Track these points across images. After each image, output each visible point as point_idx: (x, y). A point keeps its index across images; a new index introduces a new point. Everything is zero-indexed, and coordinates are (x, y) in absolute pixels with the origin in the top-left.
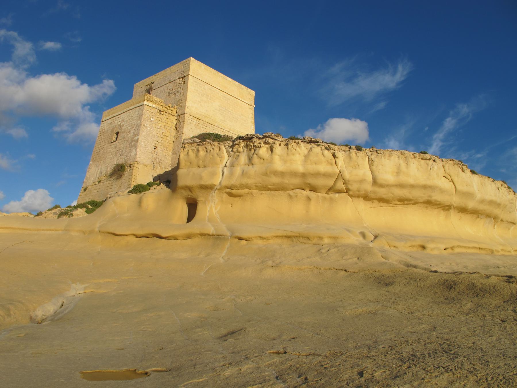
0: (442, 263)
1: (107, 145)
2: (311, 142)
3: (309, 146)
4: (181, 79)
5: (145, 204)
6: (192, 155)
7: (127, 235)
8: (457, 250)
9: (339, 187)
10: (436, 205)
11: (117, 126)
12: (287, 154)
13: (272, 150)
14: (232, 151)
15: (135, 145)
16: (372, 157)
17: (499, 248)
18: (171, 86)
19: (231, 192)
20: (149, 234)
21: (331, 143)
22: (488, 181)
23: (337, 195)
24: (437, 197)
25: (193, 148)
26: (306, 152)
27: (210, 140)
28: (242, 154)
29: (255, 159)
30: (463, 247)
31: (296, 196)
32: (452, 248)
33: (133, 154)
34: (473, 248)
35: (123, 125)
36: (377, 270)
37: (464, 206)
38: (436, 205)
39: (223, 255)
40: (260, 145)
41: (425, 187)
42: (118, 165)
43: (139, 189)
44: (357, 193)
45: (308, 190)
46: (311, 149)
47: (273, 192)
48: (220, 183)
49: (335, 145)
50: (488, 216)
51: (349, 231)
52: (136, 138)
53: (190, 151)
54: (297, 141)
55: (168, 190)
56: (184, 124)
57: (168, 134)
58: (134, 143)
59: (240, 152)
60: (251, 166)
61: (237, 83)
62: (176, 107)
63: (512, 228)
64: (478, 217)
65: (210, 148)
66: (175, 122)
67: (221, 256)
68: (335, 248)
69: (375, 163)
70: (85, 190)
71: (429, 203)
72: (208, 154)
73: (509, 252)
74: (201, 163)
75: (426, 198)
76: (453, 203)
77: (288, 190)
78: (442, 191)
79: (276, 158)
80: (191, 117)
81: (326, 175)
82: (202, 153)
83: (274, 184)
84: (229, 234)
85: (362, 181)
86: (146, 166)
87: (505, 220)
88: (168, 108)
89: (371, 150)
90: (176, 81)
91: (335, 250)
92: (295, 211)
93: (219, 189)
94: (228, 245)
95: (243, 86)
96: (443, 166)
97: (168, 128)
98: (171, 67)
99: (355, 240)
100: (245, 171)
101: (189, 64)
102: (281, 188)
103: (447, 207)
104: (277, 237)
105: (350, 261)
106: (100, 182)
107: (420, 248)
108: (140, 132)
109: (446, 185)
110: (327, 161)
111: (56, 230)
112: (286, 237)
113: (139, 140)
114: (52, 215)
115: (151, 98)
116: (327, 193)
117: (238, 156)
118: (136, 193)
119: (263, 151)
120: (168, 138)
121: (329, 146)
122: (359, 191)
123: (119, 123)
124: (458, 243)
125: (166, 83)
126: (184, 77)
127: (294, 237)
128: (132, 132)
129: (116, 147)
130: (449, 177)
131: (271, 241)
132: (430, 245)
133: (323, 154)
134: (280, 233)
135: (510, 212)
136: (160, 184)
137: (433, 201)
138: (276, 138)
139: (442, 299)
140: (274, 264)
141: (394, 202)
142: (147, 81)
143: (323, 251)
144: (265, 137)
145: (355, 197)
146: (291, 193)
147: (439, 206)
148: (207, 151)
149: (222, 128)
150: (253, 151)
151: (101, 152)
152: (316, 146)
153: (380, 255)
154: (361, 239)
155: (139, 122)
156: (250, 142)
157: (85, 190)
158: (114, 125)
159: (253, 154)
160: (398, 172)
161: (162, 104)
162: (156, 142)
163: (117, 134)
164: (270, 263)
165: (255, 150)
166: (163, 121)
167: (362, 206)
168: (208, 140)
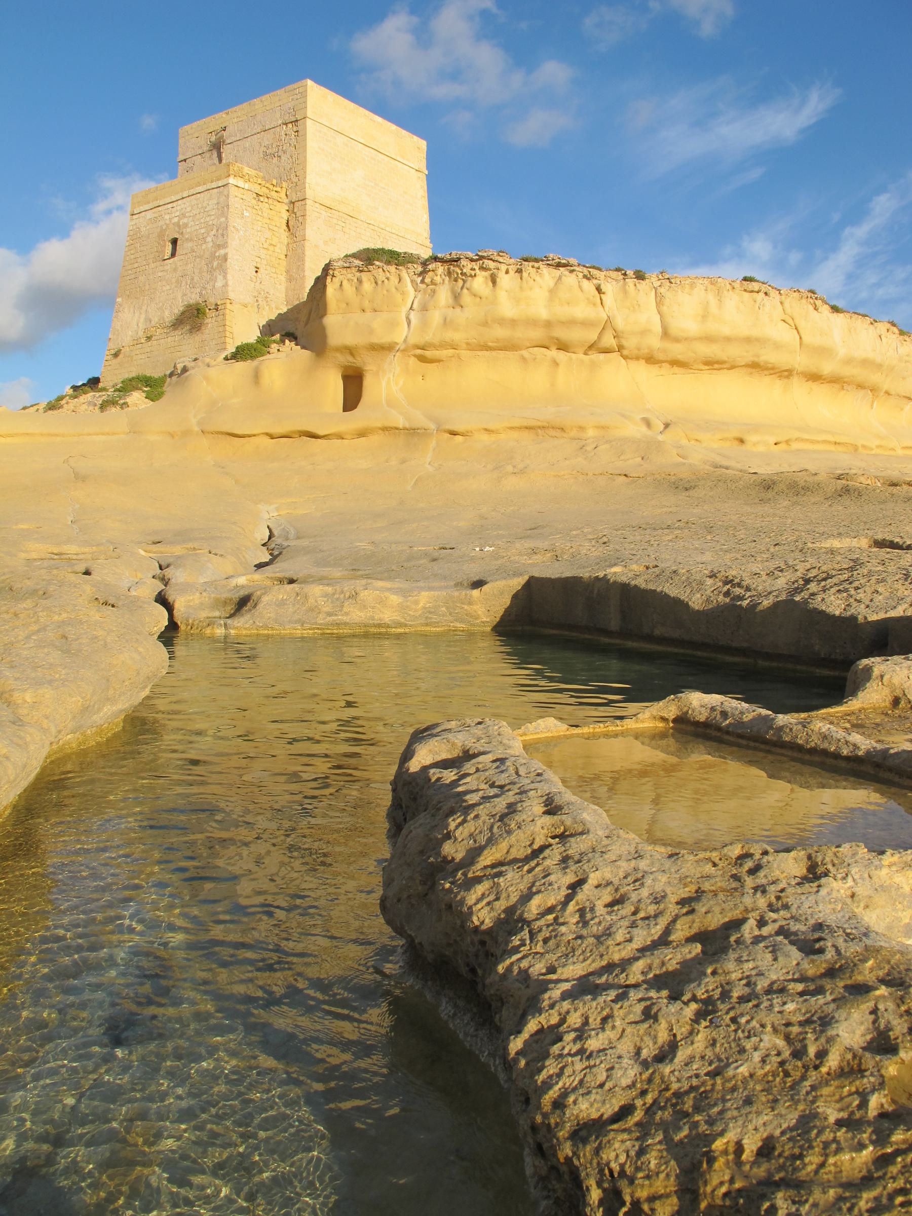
0: (768, 464)
1: (152, 265)
2: (559, 265)
3: (557, 273)
4: (290, 126)
5: (266, 380)
6: (348, 288)
7: (254, 435)
8: (795, 446)
9: (606, 344)
10: (767, 369)
11: (171, 226)
12: (521, 288)
13: (494, 282)
14: (423, 282)
15: (220, 266)
16: (662, 290)
17: (874, 443)
18: (267, 139)
19: (424, 355)
20: (294, 432)
21: (594, 267)
22: (861, 324)
23: (602, 356)
24: (768, 356)
25: (350, 276)
26: (551, 283)
27: (382, 261)
28: (442, 288)
29: (466, 298)
30: (807, 440)
31: (535, 359)
32: (787, 442)
33: (219, 284)
34: (825, 442)
35: (186, 225)
36: (672, 474)
37: (815, 370)
38: (767, 369)
39: (429, 460)
40: (473, 273)
41: (748, 340)
42: (189, 306)
43: (242, 353)
44: (636, 352)
45: (554, 349)
46: (560, 278)
47: (494, 353)
48: (405, 341)
49: (600, 270)
50: (860, 386)
51: (623, 416)
52: (222, 252)
53: (345, 283)
54: (536, 265)
55: (306, 353)
56: (305, 220)
57: (275, 241)
58: (218, 263)
59: (436, 285)
60: (458, 310)
61: (394, 127)
62: (284, 185)
63: (909, 407)
64: (843, 389)
65: (381, 276)
66: (285, 215)
67: (425, 460)
68: (607, 442)
69: (667, 302)
70: (116, 355)
71: (755, 366)
72: (379, 288)
73: (893, 449)
74: (366, 304)
75: (749, 358)
76: (797, 366)
77: (521, 350)
78: (777, 346)
79: (502, 295)
80: (317, 205)
81: (586, 324)
82: (367, 286)
83: (498, 340)
84: (432, 426)
85: (644, 332)
86: (245, 306)
87: (893, 392)
88: (271, 187)
89: (660, 277)
90: (278, 129)
91: (607, 446)
92: (534, 382)
93: (403, 350)
94: (433, 443)
95: (404, 132)
96: (781, 303)
97: (275, 228)
98: (264, 98)
99: (634, 430)
100: (448, 320)
101: (304, 95)
102: (509, 346)
103: (786, 373)
104: (511, 428)
105: (631, 462)
106: (149, 338)
107: (737, 443)
108: (229, 241)
109: (785, 335)
110: (588, 299)
111: (114, 434)
112: (526, 428)
113: (229, 256)
114: (85, 407)
115: (241, 170)
116: (585, 354)
117: (434, 291)
118: (244, 359)
119: (480, 282)
120: (277, 249)
121: (590, 272)
122: (639, 349)
123: (176, 220)
124: (797, 434)
125: (255, 131)
126: (296, 122)
127: (539, 427)
128: (209, 239)
129: (175, 270)
130: (791, 322)
131: (502, 436)
132: (751, 438)
133: (580, 287)
134: (516, 424)
135: (904, 378)
136: (283, 342)
137: (762, 364)
138: (501, 259)
139: (757, 501)
140: (516, 471)
141: (696, 366)
142: (213, 122)
143: (589, 448)
144: (482, 258)
145: (631, 359)
146: (525, 353)
147: (772, 372)
148: (376, 283)
149: (372, 222)
150: (460, 283)
151: (142, 278)
152: (567, 273)
153: (675, 452)
154: (643, 428)
155: (223, 219)
156: (454, 266)
157: (116, 355)
158: (160, 224)
159: (462, 288)
160: (705, 316)
161: (260, 181)
162: (258, 260)
163: (174, 242)
164: (510, 468)
165: (464, 281)
166: (265, 215)
167: (642, 372)
168: (377, 263)
